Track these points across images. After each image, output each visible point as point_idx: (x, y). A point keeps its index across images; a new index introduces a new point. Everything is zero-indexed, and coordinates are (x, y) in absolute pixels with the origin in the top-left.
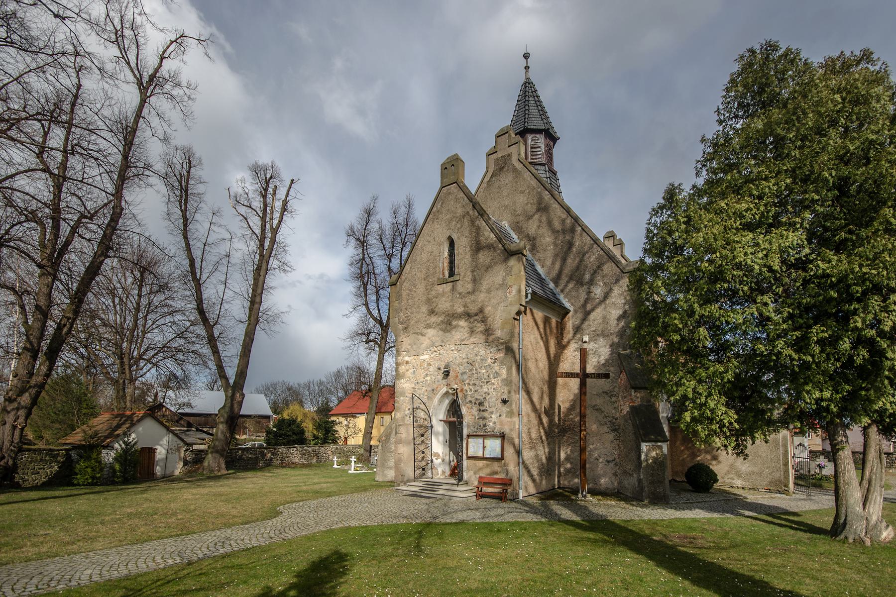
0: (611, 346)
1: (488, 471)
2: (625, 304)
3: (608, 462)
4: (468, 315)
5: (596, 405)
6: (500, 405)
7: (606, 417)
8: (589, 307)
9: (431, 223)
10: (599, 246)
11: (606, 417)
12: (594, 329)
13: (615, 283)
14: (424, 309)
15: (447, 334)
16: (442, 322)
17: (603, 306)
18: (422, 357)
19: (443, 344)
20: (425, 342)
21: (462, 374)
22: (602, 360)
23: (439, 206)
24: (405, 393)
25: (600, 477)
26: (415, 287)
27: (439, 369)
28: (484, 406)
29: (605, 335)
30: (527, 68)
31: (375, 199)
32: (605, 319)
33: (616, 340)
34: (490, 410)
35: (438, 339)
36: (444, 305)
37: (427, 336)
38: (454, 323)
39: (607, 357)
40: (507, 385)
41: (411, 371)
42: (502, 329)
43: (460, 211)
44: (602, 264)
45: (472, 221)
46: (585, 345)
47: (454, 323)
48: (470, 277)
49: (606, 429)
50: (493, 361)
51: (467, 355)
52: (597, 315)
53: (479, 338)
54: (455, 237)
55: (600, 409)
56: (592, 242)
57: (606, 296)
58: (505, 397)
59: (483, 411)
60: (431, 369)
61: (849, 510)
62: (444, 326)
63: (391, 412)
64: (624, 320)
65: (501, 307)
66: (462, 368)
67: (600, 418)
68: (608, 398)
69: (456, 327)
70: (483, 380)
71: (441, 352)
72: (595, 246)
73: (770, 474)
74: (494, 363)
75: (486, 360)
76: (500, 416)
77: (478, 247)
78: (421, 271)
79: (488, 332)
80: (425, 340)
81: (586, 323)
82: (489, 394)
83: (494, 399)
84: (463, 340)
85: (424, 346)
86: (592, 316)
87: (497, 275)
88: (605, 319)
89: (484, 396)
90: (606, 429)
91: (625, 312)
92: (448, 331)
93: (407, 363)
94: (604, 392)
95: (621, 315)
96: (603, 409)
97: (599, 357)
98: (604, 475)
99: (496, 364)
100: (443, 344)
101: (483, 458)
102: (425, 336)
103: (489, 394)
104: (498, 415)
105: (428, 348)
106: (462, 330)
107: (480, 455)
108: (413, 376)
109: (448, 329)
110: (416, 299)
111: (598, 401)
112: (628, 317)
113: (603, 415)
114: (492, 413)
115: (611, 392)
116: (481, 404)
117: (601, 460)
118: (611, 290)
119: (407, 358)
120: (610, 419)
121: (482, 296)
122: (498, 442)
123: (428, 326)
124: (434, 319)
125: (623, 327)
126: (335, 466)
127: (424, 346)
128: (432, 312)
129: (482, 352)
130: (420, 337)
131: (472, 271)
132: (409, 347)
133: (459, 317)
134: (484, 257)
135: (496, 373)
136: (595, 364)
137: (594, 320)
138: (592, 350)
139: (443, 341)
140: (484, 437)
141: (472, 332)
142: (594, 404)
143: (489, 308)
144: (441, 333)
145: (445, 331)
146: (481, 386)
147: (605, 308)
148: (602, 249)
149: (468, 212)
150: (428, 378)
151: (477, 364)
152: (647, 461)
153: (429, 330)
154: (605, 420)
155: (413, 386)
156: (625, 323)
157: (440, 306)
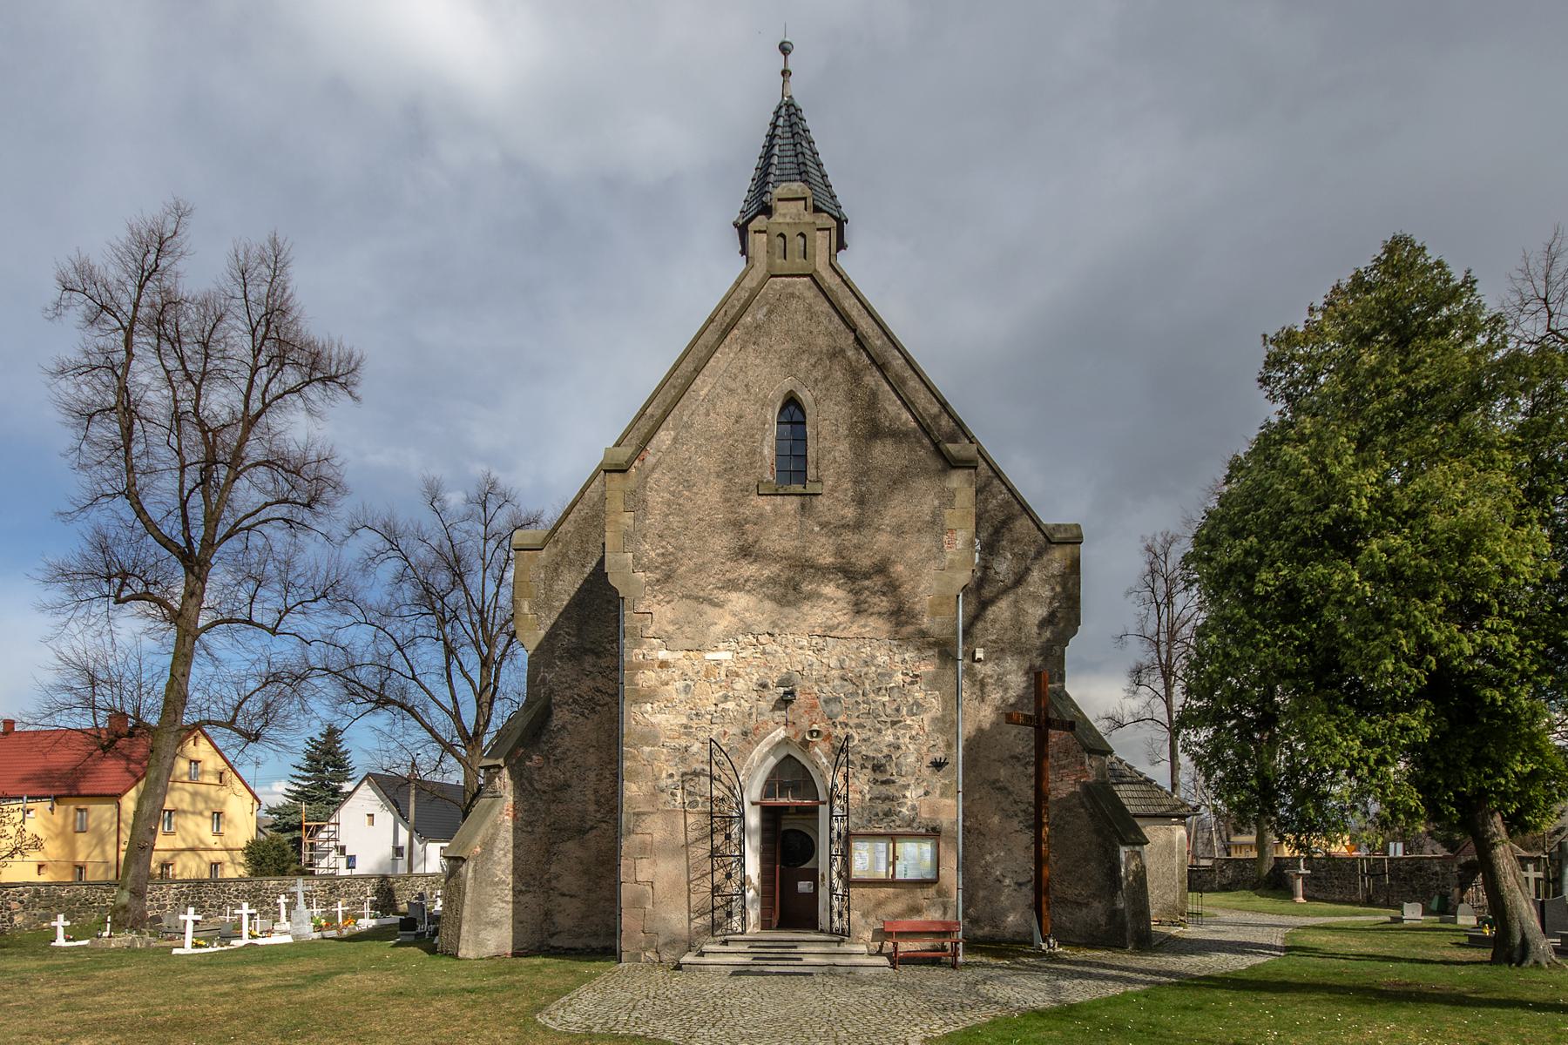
0: (1027, 673)
1: (896, 907)
2: (1053, 598)
3: (1020, 885)
4: (847, 573)
5: (997, 781)
6: (926, 772)
7: (1016, 802)
8: (987, 592)
9: (736, 348)
10: (1004, 483)
11: (1016, 802)
12: (994, 637)
13: (1035, 558)
14: (721, 543)
15: (786, 610)
16: (773, 581)
17: (1011, 597)
18: (709, 656)
19: (777, 631)
20: (722, 622)
21: (827, 701)
22: (1012, 697)
23: (760, 316)
24: (656, 737)
25: (1004, 912)
26: (689, 488)
27: (764, 686)
28: (885, 771)
29: (1020, 650)
30: (785, 73)
31: (180, 213)
32: (1018, 624)
33: (1038, 662)
34: (901, 781)
35: (760, 618)
36: (777, 539)
37: (728, 607)
38: (807, 587)
39: (1020, 692)
40: (942, 731)
41: (680, 684)
42: (934, 614)
43: (822, 342)
44: (1009, 518)
45: (855, 375)
46: (977, 666)
47: (807, 587)
48: (850, 493)
49: (1015, 824)
50: (908, 680)
51: (841, 662)
52: (1002, 610)
53: (875, 626)
54: (806, 396)
55: (1006, 789)
56: (990, 473)
57: (1020, 579)
58: (939, 755)
59: (884, 783)
60: (740, 685)
61: (1525, 926)
62: (779, 591)
63: (120, 796)
64: (1051, 627)
65: (931, 569)
66: (827, 689)
67: (1006, 804)
68: (1020, 769)
69: (813, 596)
70: (884, 718)
71: (768, 648)
72: (996, 482)
73: (1162, 897)
74: (912, 683)
75: (891, 676)
76: (926, 793)
77: (871, 430)
78: (707, 454)
79: (900, 615)
80: (721, 617)
81: (980, 625)
82: (898, 748)
83: (911, 759)
84: (832, 628)
85: (718, 629)
86: (991, 613)
87: (922, 499)
88: (1018, 624)
89: (886, 751)
90: (1015, 824)
91: (1052, 614)
92: (789, 604)
93: (664, 664)
94: (1013, 757)
95: (1044, 619)
96: (1011, 789)
97: (1006, 690)
98: (1013, 908)
99: (916, 687)
100: (777, 631)
101: (891, 882)
102: (721, 606)
103: (898, 748)
104: (921, 791)
105: (728, 636)
106: (829, 605)
107: (882, 874)
108: (682, 697)
109: (791, 597)
110: (693, 518)
111: (1002, 772)
112: (1058, 623)
113: (1011, 798)
114: (906, 787)
115: (1025, 757)
116: (878, 768)
117: (1007, 881)
118: (1028, 570)
119: (663, 655)
120: (1023, 807)
121: (883, 540)
122: (927, 847)
123: (732, 585)
124: (749, 569)
125: (1048, 640)
126: (60, 941)
127: (718, 629)
128: (745, 552)
129: (882, 658)
130: (706, 607)
131: (856, 482)
132: (670, 628)
133: (823, 572)
134: (884, 454)
135: (916, 703)
136: (998, 703)
137: (994, 621)
138: (991, 677)
139: (774, 624)
140: (893, 837)
141: (858, 609)
142: (994, 777)
143: (900, 568)
144: (768, 605)
145: (782, 601)
146: (879, 731)
147: (1016, 601)
148: (1009, 490)
149: (842, 351)
150: (730, 705)
151: (867, 682)
152: (1127, 877)
153: (734, 596)
154: (1016, 808)
155: (684, 721)
156: (1052, 632)
157: (765, 543)
